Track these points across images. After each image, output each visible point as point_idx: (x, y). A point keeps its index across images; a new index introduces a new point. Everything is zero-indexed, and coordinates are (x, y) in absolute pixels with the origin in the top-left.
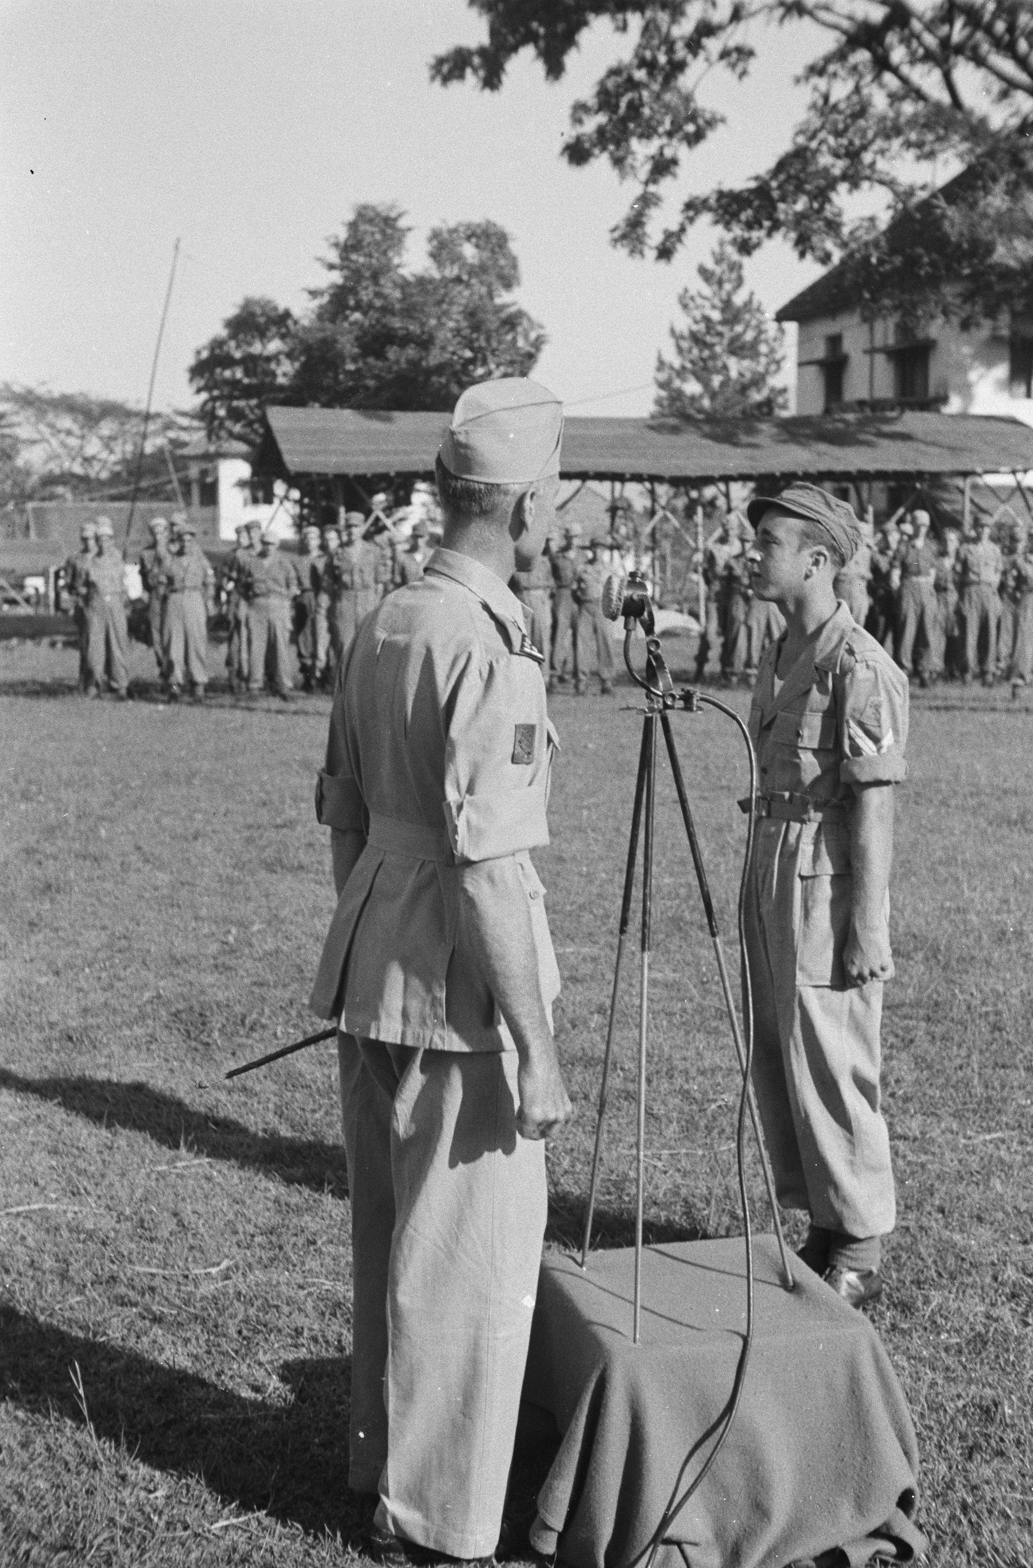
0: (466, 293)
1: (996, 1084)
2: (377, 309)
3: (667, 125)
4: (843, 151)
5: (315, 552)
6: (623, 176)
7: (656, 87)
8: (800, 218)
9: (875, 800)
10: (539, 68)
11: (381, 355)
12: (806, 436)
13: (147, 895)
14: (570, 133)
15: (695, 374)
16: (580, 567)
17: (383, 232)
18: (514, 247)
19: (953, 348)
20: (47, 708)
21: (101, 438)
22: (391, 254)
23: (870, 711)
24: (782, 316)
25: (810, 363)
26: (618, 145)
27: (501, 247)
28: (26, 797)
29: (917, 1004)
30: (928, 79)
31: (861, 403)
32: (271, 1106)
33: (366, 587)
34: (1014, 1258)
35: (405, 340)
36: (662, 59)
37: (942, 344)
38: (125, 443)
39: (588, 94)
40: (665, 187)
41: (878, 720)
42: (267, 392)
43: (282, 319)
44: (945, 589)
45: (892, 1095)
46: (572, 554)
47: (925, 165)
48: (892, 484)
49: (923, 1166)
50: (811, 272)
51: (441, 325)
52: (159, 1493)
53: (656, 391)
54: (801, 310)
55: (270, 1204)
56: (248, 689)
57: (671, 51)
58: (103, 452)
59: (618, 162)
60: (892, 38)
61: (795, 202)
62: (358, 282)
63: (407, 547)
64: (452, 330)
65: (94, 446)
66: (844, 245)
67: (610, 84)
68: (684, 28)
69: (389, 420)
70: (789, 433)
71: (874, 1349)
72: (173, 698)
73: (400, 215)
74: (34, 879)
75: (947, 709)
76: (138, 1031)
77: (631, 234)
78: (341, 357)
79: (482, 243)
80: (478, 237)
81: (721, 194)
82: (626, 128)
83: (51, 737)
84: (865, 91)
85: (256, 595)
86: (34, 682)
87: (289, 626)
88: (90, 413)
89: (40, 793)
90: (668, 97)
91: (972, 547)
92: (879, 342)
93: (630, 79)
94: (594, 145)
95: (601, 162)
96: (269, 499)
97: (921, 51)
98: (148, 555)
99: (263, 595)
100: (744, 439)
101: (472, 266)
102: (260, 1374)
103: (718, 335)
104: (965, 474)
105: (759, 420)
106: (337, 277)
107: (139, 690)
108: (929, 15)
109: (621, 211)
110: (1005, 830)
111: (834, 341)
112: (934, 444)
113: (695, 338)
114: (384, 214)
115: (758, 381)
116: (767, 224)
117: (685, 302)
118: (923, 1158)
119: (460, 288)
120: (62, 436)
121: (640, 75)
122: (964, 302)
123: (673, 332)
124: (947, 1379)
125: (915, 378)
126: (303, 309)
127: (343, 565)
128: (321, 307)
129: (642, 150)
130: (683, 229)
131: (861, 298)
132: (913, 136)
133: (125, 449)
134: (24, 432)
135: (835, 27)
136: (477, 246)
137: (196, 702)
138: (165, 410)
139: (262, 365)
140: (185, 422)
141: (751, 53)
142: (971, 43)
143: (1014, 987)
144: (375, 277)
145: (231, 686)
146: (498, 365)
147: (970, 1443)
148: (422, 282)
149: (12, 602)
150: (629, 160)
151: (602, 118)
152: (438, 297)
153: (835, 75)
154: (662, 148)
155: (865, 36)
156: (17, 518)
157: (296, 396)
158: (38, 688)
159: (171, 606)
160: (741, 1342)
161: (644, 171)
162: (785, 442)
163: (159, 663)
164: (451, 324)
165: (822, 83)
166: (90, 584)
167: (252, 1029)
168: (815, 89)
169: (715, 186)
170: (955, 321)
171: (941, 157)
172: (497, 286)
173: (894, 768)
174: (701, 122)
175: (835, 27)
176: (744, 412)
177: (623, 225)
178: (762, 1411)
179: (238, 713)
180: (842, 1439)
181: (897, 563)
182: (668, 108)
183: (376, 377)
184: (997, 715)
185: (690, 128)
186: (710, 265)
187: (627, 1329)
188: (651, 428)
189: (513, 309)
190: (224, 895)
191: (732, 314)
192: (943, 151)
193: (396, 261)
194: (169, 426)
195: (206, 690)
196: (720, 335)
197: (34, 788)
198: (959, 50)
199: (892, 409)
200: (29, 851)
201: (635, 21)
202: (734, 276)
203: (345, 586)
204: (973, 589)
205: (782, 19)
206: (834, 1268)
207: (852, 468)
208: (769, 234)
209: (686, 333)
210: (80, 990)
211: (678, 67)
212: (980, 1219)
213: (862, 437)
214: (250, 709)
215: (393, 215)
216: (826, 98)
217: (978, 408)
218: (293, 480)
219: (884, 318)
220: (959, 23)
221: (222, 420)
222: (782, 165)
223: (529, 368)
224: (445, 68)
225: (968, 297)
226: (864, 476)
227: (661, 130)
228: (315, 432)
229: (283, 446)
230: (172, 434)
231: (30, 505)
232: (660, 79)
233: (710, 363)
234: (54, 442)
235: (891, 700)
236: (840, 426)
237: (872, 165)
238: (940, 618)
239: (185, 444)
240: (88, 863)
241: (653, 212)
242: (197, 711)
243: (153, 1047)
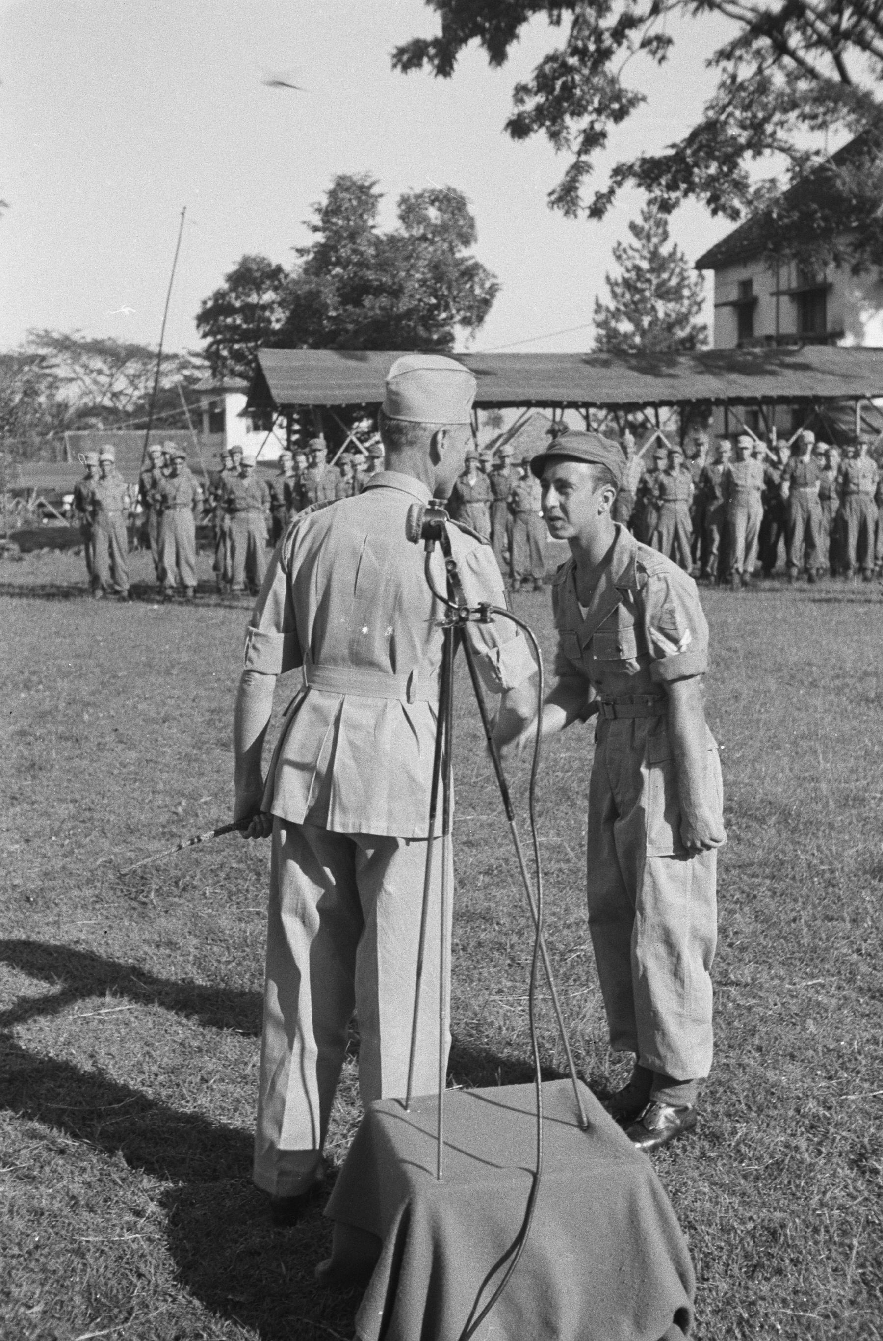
0: (431, 249)
1: (824, 936)
2: (355, 264)
3: (596, 104)
4: (748, 122)
5: (289, 473)
7: (586, 71)
8: (712, 179)
10: (484, 55)
11: (358, 303)
12: (719, 367)
13: (116, 772)
14: (510, 110)
16: (515, 484)
17: (359, 199)
18: (472, 209)
19: (847, 293)
20: (57, 609)
21: (127, 376)
22: (365, 217)
23: (666, 617)
24: (701, 265)
25: (724, 304)
26: (554, 122)
27: (459, 209)
28: (27, 687)
29: (764, 864)
30: (821, 61)
31: (769, 338)
32: (191, 958)
34: (816, 1093)
35: (379, 290)
36: (592, 47)
37: (837, 287)
38: (147, 380)
39: (528, 78)
40: (595, 156)
41: (674, 624)
42: (261, 335)
43: (275, 273)
44: (829, 498)
45: (731, 945)
46: (505, 472)
47: (819, 134)
48: (796, 407)
49: (749, 1009)
50: (722, 228)
51: (409, 276)
52: (37, 1309)
53: (594, 331)
54: (717, 259)
55: (176, 1046)
56: (232, 591)
57: (599, 40)
58: (129, 388)
59: (554, 135)
60: (790, 26)
61: (707, 167)
62: (339, 241)
63: (365, 467)
64: (419, 281)
65: (121, 384)
66: (749, 203)
67: (547, 68)
68: (610, 21)
69: (363, 359)
70: (706, 365)
71: (650, 1182)
72: (168, 599)
73: (373, 184)
74: (22, 757)
75: (828, 601)
76: (88, 892)
77: (566, 196)
78: (326, 307)
79: (443, 207)
80: (441, 202)
81: (644, 161)
82: (561, 106)
83: (57, 633)
84: (767, 72)
85: (238, 510)
86: (52, 586)
87: (266, 536)
88: (117, 355)
89: (40, 682)
90: (595, 80)
91: (852, 462)
92: (784, 286)
93: (564, 64)
94: (534, 121)
95: (539, 137)
96: (269, 427)
97: (815, 37)
98: (146, 477)
99: (243, 510)
100: (665, 370)
101: (436, 226)
102: (142, 1199)
103: (646, 281)
104: (857, 398)
105: (680, 355)
106: (320, 237)
107: (139, 592)
108: (822, 7)
109: (557, 178)
110: (863, 708)
111: (746, 285)
112: (832, 373)
113: (627, 283)
114: (359, 183)
115: (682, 320)
116: (683, 186)
117: (619, 254)
118: (752, 1002)
119: (424, 245)
120: (94, 374)
121: (573, 61)
122: (855, 251)
123: (608, 278)
124: (743, 1203)
125: (816, 317)
126: (293, 265)
128: (307, 263)
129: (575, 126)
130: (612, 192)
132: (807, 109)
133: (146, 385)
134: (62, 372)
135: (740, 18)
136: (440, 209)
137: (188, 602)
138: (182, 352)
139: (259, 312)
140: (197, 361)
141: (669, 41)
142: (859, 29)
143: (853, 849)
144: (352, 236)
145: (216, 589)
146: (458, 311)
147: (755, 1262)
148: (393, 240)
149: (51, 516)
150: (564, 134)
151: (540, 99)
152: (407, 253)
153: (740, 58)
154: (592, 123)
155: (767, 25)
156: (57, 444)
157: (285, 340)
158: (54, 590)
159: (166, 520)
160: (532, 1179)
161: (576, 143)
162: (701, 373)
163: (157, 568)
164: (418, 276)
165: (730, 65)
166: (96, 503)
167: (184, 890)
168: (724, 70)
169: (639, 155)
170: (847, 267)
171: (832, 127)
172: (457, 243)
174: (624, 101)
175: (740, 18)
176: (669, 347)
177: (558, 189)
179: (221, 612)
180: (622, 1264)
181: (787, 476)
182: (597, 90)
183: (353, 322)
184: (872, 606)
185: (616, 106)
186: (639, 221)
187: (433, 1168)
188: (587, 362)
189: (471, 262)
190: (181, 771)
191: (659, 263)
192: (832, 122)
193: (371, 223)
194: (184, 365)
195: (195, 591)
196: (649, 281)
197: (35, 678)
198: (847, 35)
199: (795, 343)
200: (22, 733)
201: (567, 16)
202: (660, 230)
204: (854, 497)
205: (696, 10)
206: (654, 1103)
207: (758, 395)
208: (686, 195)
209: (620, 280)
210: (44, 856)
211: (605, 54)
212: (792, 1057)
213: (769, 367)
214: (230, 607)
215: (367, 184)
216: (734, 77)
217: (870, 341)
218: (286, 410)
219: (789, 264)
220: (847, 13)
221: (225, 358)
222: (694, 135)
223: (485, 312)
224: (405, 58)
225: (858, 246)
226: (768, 400)
227: (590, 108)
228: (297, 369)
229: (271, 382)
230: (187, 372)
231: (67, 434)
232: (589, 64)
233: (640, 306)
234: (88, 380)
235: (684, 606)
236: (749, 358)
237: (774, 133)
238: (825, 523)
239: (198, 380)
240: (69, 744)
241: (585, 178)
242: (186, 610)
243: (98, 906)
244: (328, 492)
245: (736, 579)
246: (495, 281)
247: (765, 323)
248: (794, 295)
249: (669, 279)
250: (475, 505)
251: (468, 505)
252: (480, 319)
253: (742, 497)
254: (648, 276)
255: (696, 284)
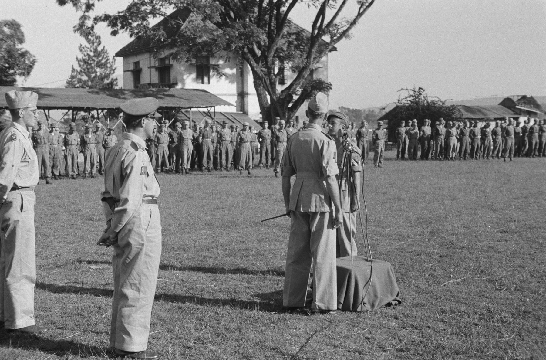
6: (77, 9)
9: (357, 174)
15: (85, 73)
18: (22, 29)
19: (178, 68)
24: (118, 55)
27: (18, 29)
33: (45, 143)
54: (124, 53)
80: (8, 25)
92: (152, 65)
109: (77, 22)
111: (137, 64)
113: (84, 60)
115: (107, 76)
123: (77, 59)
127: (38, 137)
131: (153, 51)
161: (84, 7)
162: (135, 97)
173: (360, 169)
176: (103, 86)
177: (78, 26)
178: (375, 279)
181: (201, 135)
189: (23, 50)
191: (98, 54)
196: (93, 60)
202: (98, 41)
203: (39, 143)
213: (159, 96)
217: (187, 87)
222: (129, 8)
223: (31, 71)
244: (45, 139)
245: (184, 171)
246: (34, 58)
247: (145, 79)
248: (157, 69)
249: (102, 60)
250: (91, 145)
251: (70, 146)
252: (29, 73)
253: (186, 142)
254: (93, 58)
255: (112, 62)
